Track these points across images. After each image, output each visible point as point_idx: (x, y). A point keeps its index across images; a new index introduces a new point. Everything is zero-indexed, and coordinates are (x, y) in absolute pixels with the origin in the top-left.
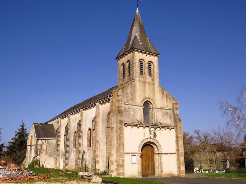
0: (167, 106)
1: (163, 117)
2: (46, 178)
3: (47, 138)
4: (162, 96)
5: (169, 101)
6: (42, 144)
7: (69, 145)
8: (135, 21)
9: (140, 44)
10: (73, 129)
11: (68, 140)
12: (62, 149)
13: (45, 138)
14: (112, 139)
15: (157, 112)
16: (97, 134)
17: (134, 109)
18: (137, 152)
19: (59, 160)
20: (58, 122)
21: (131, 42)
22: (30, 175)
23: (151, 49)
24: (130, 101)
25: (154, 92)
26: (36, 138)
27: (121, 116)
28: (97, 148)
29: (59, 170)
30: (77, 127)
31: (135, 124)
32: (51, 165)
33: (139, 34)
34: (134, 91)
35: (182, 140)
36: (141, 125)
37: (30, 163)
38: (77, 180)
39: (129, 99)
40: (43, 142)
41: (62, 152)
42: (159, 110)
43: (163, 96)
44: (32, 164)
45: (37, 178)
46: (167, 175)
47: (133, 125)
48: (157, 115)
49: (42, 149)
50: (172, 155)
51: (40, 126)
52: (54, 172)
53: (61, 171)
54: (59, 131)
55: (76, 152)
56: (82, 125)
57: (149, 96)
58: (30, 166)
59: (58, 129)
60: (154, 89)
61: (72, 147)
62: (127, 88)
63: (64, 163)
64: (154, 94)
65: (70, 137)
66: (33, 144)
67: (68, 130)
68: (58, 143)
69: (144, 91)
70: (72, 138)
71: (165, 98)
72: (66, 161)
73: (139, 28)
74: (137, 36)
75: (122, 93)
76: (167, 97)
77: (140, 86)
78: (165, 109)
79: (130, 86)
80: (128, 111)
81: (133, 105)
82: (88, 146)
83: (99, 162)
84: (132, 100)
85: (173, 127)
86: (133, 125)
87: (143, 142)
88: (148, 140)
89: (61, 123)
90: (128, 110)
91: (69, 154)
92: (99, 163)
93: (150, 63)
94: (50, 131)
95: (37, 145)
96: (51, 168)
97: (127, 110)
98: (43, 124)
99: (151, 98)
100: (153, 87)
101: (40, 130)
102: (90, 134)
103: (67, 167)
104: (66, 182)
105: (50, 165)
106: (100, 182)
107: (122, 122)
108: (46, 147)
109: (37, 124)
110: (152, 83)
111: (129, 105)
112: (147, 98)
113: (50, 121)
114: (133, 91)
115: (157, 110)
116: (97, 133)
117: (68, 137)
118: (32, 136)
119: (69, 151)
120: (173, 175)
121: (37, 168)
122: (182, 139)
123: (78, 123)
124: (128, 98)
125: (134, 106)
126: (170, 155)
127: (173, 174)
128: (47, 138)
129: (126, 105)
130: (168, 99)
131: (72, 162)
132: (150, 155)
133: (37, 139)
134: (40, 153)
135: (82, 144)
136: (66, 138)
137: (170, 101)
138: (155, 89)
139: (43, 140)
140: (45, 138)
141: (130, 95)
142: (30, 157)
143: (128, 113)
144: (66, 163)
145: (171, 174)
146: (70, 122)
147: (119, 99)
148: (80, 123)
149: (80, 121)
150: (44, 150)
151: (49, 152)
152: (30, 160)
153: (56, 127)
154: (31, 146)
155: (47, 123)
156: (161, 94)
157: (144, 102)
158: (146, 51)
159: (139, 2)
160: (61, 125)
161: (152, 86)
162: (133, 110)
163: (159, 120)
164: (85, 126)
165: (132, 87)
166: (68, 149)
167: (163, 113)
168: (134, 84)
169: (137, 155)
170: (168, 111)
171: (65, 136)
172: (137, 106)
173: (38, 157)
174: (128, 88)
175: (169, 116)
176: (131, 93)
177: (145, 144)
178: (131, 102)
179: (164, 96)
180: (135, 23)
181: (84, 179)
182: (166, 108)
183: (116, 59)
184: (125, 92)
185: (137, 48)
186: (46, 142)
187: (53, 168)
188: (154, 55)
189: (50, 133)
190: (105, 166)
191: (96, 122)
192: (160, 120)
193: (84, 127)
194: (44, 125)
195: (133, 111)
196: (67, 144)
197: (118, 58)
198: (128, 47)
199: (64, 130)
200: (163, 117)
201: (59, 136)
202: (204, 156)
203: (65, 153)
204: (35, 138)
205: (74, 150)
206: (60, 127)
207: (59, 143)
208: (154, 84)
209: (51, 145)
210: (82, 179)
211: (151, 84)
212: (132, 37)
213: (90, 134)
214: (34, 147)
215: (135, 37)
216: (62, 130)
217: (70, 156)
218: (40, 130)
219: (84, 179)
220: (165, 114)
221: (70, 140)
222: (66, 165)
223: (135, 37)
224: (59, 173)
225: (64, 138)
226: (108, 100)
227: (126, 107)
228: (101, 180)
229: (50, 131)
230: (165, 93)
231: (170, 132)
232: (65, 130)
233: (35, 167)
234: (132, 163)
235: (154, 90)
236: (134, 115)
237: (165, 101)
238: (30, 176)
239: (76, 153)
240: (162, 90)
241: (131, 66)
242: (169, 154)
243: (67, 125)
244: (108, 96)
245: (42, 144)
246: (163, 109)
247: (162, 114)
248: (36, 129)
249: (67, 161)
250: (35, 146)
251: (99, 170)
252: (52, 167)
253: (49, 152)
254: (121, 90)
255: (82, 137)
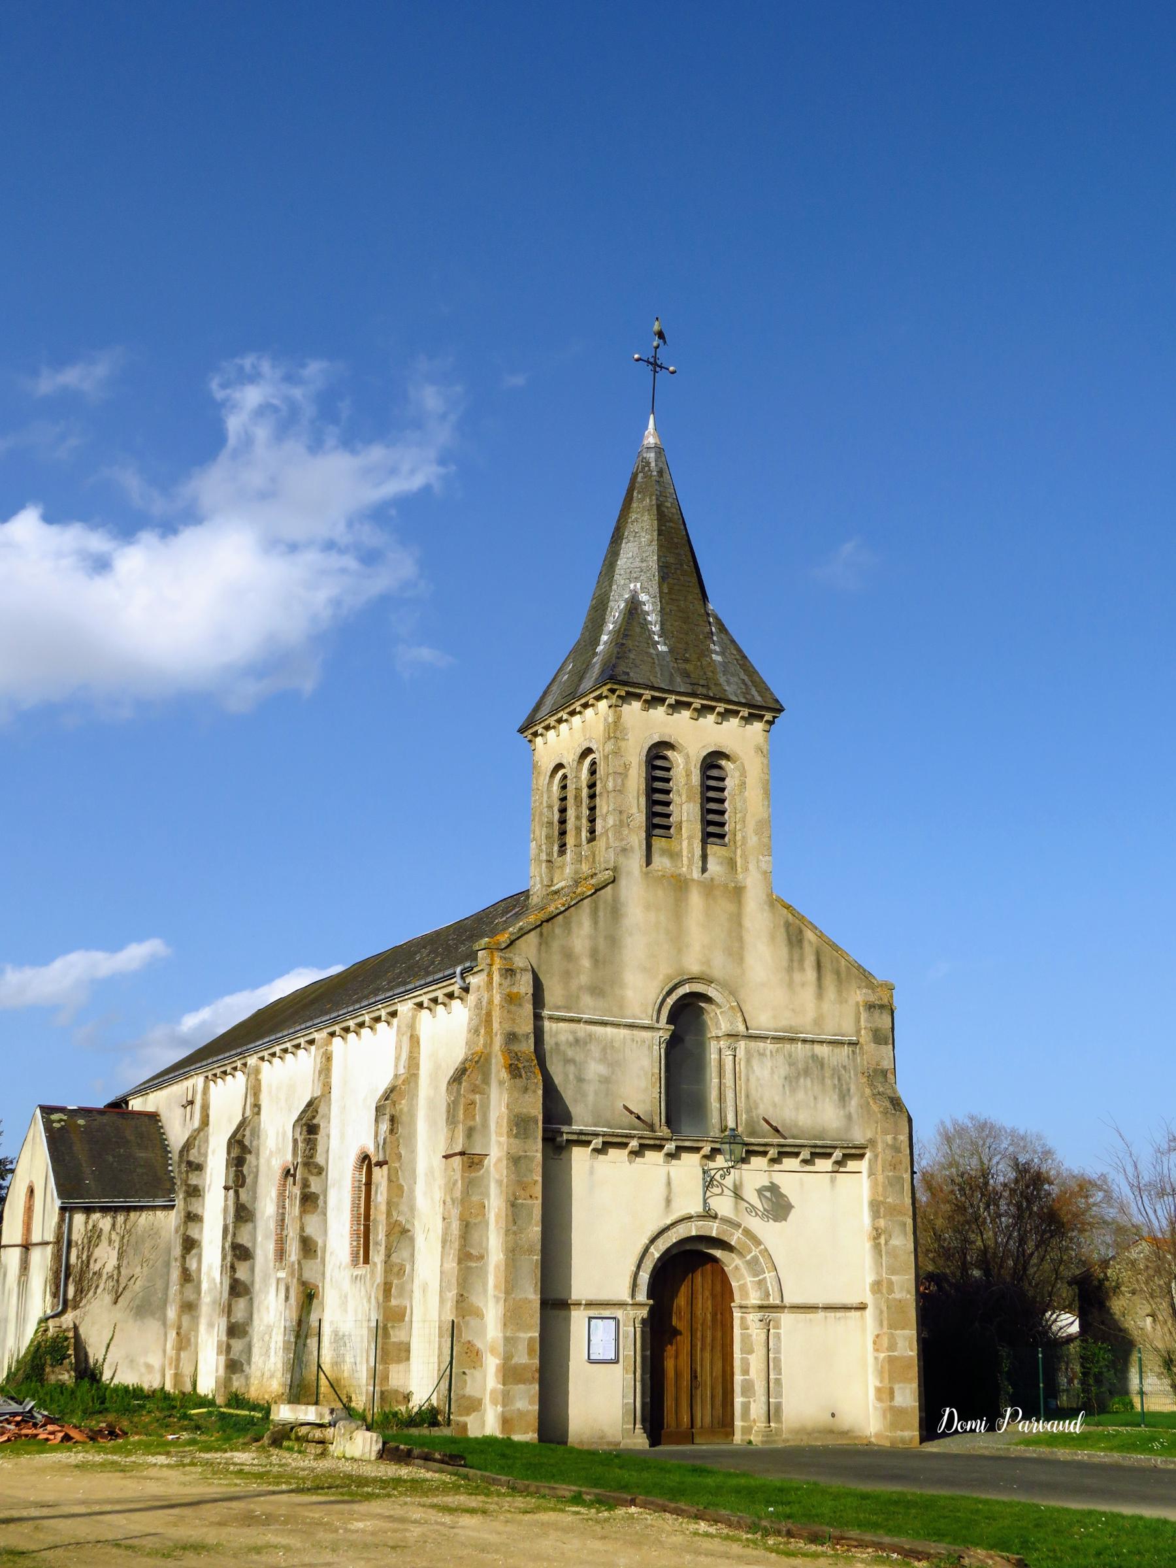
0: (818, 1021)
1: (793, 1090)
2: (104, 1437)
3: (119, 1202)
4: (791, 960)
5: (831, 992)
6: (94, 1237)
7: (249, 1245)
8: (634, 505)
9: (659, 654)
10: (274, 1149)
11: (242, 1214)
12: (210, 1267)
13: (106, 1202)
14: (473, 1220)
15: (755, 1063)
16: (401, 1187)
17: (607, 1047)
18: (625, 1296)
19: (197, 1337)
20: (191, 1103)
21: (604, 638)
22: (19, 1418)
23: (722, 679)
24: (587, 1000)
25: (740, 939)
26: (58, 1203)
27: (526, 1090)
28: (401, 1271)
29: (194, 1399)
30: (295, 1141)
31: (613, 1135)
32: (149, 1367)
33: (655, 589)
34: (614, 942)
35: (905, 1224)
36: (651, 1142)
37: (22, 1354)
38: (263, 1447)
39: (580, 988)
40: (101, 1225)
41: (210, 1290)
42: (769, 1046)
43: (794, 964)
44: (34, 1358)
45: (53, 1433)
46: (809, 1434)
47: (600, 1140)
48: (753, 1079)
49: (94, 1267)
50: (839, 1314)
51: (81, 1122)
52: (162, 1410)
53: (203, 1402)
54: (193, 1156)
55: (287, 1289)
56: (322, 1132)
57: (707, 963)
58: (18, 1370)
59: (187, 1146)
60: (737, 920)
61: (266, 1257)
62: (567, 925)
63: (222, 1358)
64: (736, 948)
65: (254, 1198)
66: (36, 1238)
67: (248, 1157)
68: (190, 1233)
69: (677, 938)
70: (267, 1207)
71: (810, 974)
72: (233, 1342)
73: (655, 547)
74: (643, 597)
75: (539, 950)
76: (819, 966)
77: (648, 907)
78: (804, 1041)
79: (588, 910)
80: (572, 1061)
81: (604, 1024)
82: (355, 1256)
83: (408, 1351)
84: (597, 991)
85: (853, 1151)
86: (600, 1140)
87: (660, 1241)
88: (693, 1229)
89: (205, 1108)
90: (570, 1053)
91: (251, 1299)
92: (408, 1359)
93: (713, 763)
94: (142, 1155)
95: (62, 1243)
96: (146, 1387)
97: (564, 1053)
98: (100, 1112)
99: (717, 972)
100: (731, 907)
101: (80, 1150)
102: (368, 1184)
103: (237, 1383)
104: (202, 1455)
105: (143, 1370)
106: (373, 1458)
107: (532, 1126)
108: (115, 1254)
109: (62, 1110)
110: (726, 886)
111: (579, 1021)
112: (691, 980)
113: (143, 1089)
114: (606, 938)
115: (753, 1044)
116: (402, 1181)
117: (244, 1196)
118: (31, 1191)
119: (253, 1282)
120: (844, 1433)
121: (62, 1386)
122: (910, 1221)
123: (299, 1119)
124: (574, 985)
125: (609, 1030)
126: (831, 1315)
127: (846, 1427)
128: (119, 1202)
129: (562, 1025)
130: (829, 981)
131: (267, 1354)
132: (709, 1317)
133: (63, 1209)
134: (80, 1291)
135: (320, 1243)
136: (231, 1203)
137: (839, 992)
138: (747, 923)
139: (96, 1216)
140: (106, 1202)
141: (586, 963)
142: (21, 1319)
143: (571, 1069)
144: (234, 1355)
145: (831, 1432)
146: (257, 1106)
147: (515, 990)
148: (309, 1114)
149: (310, 1104)
150: (104, 1277)
151: (138, 1286)
152: (19, 1338)
153: (176, 1132)
154: (26, 1247)
155: (119, 1106)
156: (784, 951)
157: (670, 1001)
158: (694, 695)
159: (662, 374)
160: (205, 1121)
161: (724, 906)
162: (604, 1050)
163: (764, 1109)
164: (342, 1135)
165: (601, 914)
166: (242, 1274)
167: (790, 1065)
168: (609, 897)
169: (619, 1313)
170: (822, 1051)
171: (227, 1188)
172: (632, 1026)
173: (68, 1319)
174: (574, 926)
175: (828, 1082)
176: (594, 954)
177: (674, 1252)
178: (589, 1007)
179: (801, 961)
180: (634, 516)
181: (298, 1439)
182: (810, 1036)
183: (522, 730)
184: (556, 945)
185: (634, 677)
186: (118, 1226)
187: (156, 1385)
188: (745, 712)
189: (139, 1170)
190: (436, 1375)
191: (393, 1119)
192: (775, 1105)
193: (334, 1143)
194: (104, 1119)
195: (603, 1059)
196: (240, 1240)
197: (530, 727)
198: (588, 666)
199: (225, 1155)
200: (793, 1090)
201: (194, 1192)
202: (1154, 1321)
203: (226, 1295)
204: (49, 1203)
205: (278, 1280)
206: (199, 1130)
207: (193, 1233)
208: (737, 892)
209: (148, 1244)
210: (290, 1443)
211: (717, 893)
212: (611, 604)
213: (368, 1184)
214: (44, 1257)
215: (634, 608)
216: (213, 1152)
217: (255, 1316)
218: (80, 1150)
219: (298, 1439)
220: (807, 1072)
221: (258, 1215)
222: (234, 1366)
223: (634, 608)
224: (189, 1418)
225: (222, 1204)
226: (456, 989)
227: (562, 1038)
228: (380, 1445)
229: (142, 1155)
230: (806, 945)
231: (833, 1181)
232: (229, 1153)
233: (52, 1379)
234: (591, 1361)
235: (740, 925)
236: (605, 1080)
237: (808, 995)
238: (18, 1424)
239: (287, 1298)
240: (788, 925)
241: (598, 783)
242: (828, 1308)
243: (242, 1125)
244: (458, 970)
245: (94, 1237)
246: (792, 1040)
247: (783, 1070)
248: (58, 1142)
249: (238, 1345)
250: (49, 1248)
251: (407, 1398)
252: (150, 1382)
253: (138, 1286)
254: (533, 937)
255: (320, 1202)
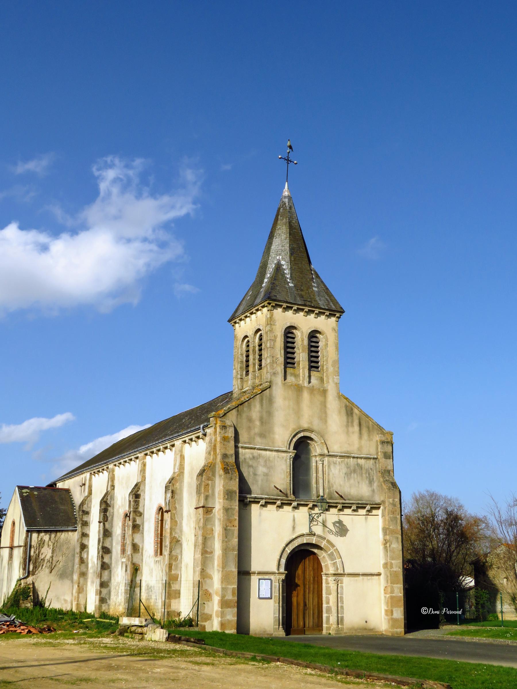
0: (360, 449)
1: (349, 479)
2: (46, 631)
3: (52, 528)
4: (348, 422)
5: (365, 436)
6: (41, 543)
7: (109, 547)
8: (279, 222)
9: (290, 287)
10: (120, 505)
11: (107, 533)
12: (92, 557)
13: (47, 528)
14: (208, 536)
15: (332, 467)
16: (176, 522)
17: (267, 460)
18: (275, 570)
19: (86, 587)
20: (84, 485)
21: (266, 280)
22: (8, 623)
23: (317, 299)
24: (258, 439)
25: (325, 413)
26: (25, 529)
27: (231, 479)
28: (176, 559)
29: (85, 615)
30: (130, 501)
31: (269, 499)
32: (66, 601)
33: (288, 259)
34: (270, 414)
35: (398, 538)
36: (286, 502)
37: (10, 595)
38: (116, 636)
39: (255, 434)
40: (44, 538)
41: (92, 567)
42: (338, 460)
43: (349, 423)
44: (15, 597)
45: (23, 630)
46: (356, 630)
47: (264, 501)
48: (331, 474)
49: (42, 557)
50: (369, 578)
51: (36, 493)
52: (71, 619)
53: (89, 616)
54: (85, 508)
55: (126, 567)
56: (142, 497)
57: (311, 423)
58: (8, 602)
59: (82, 504)
60: (324, 404)
61: (117, 552)
62: (249, 407)
63: (98, 597)
64: (324, 417)
65: (112, 526)
66: (16, 544)
67: (109, 508)
68: (84, 542)
69: (298, 412)
70: (117, 530)
71: (356, 428)
72: (102, 590)
73: (288, 240)
74: (283, 262)
75: (237, 417)
76: (360, 425)
77: (285, 399)
78: (354, 457)
79: (258, 400)
80: (251, 466)
81: (266, 450)
82: (156, 552)
83: (179, 594)
84: (262, 435)
85: (375, 506)
86: (264, 501)
87: (290, 545)
88: (304, 540)
89: (90, 487)
90: (251, 463)
91: (110, 571)
92: (179, 597)
93: (313, 335)
94: (62, 507)
95: (27, 546)
96: (64, 609)
97: (248, 463)
98: (44, 489)
99: (315, 427)
100: (321, 399)
101: (35, 506)
102: (162, 520)
103: (104, 608)
104: (89, 639)
105: (63, 602)
106: (164, 641)
107: (234, 495)
108: (50, 551)
109: (27, 488)
110: (319, 389)
111: (254, 449)
112: (304, 431)
113: (63, 479)
114: (266, 412)
115: (331, 459)
116: (177, 519)
117: (107, 526)
118: (14, 523)
119: (111, 563)
120: (371, 630)
121: (27, 609)
122: (400, 537)
123: (132, 492)
124: (252, 433)
125: (268, 453)
126: (365, 578)
127: (372, 627)
128: (52, 528)
129: (247, 450)
130: (365, 431)
131: (117, 595)
132: (312, 579)
133: (28, 531)
134: (35, 567)
135: (141, 546)
136: (101, 528)
137: (369, 436)
138: (329, 405)
139: (42, 534)
140: (47, 528)
141: (258, 423)
142: (9, 580)
143: (251, 470)
144: (103, 595)
145: (365, 629)
146: (113, 486)
147: (226, 435)
148: (136, 489)
149: (136, 485)
150: (46, 561)
151: (60, 565)
152: (8, 588)
153: (78, 498)
154: (12, 548)
155: (52, 486)
156: (345, 418)
157: (295, 440)
158: (305, 305)
159: (291, 164)
160: (90, 493)
161: (318, 398)
162: (266, 461)
163: (336, 487)
164: (151, 499)
165: (264, 401)
166: (106, 560)
167: (347, 468)
168: (268, 394)
169: (272, 577)
170: (361, 462)
171: (100, 522)
172: (278, 451)
173: (30, 580)
174: (252, 407)
175: (364, 475)
176: (261, 419)
177: (296, 550)
178: (259, 442)
179: (352, 422)
180: (279, 227)
181: (131, 632)
182: (356, 455)
183: (229, 321)
184: (244, 415)
185: (279, 297)
186: (52, 539)
187: (69, 609)
188: (327, 313)
189: (61, 514)
190: (192, 604)
191: (173, 492)
192: (341, 486)
193: (147, 502)
194: (46, 492)
195: (265, 465)
196: (105, 545)
197: (233, 319)
198: (259, 293)
199: (99, 508)
200: (349, 479)
201: (85, 524)
202: (507, 580)
203: (99, 569)
204: (21, 529)
205: (122, 562)
206: (87, 497)
207: (85, 542)
208: (324, 392)
209: (65, 547)
210: (128, 634)
211: (315, 392)
212: (269, 265)
213: (162, 520)
214: (19, 552)
215: (279, 267)
216: (94, 506)
217: (112, 578)
218: (35, 506)
219: (131, 632)
220: (355, 471)
221: (114, 534)
222: (103, 600)
223: (279, 267)
224: (83, 623)
225: (98, 529)
226: (200, 434)
227: (247, 456)
228: (167, 635)
229: (62, 507)
230: (354, 415)
231: (366, 519)
232: (100, 507)
233: (23, 606)
234: (260, 598)
235: (325, 406)
236: (266, 475)
237: (355, 437)
238: (8, 626)
239: (126, 570)
240: (346, 407)
241: (263, 344)
242: (364, 575)
243: (106, 494)
244: (202, 426)
245: (41, 543)
246: (348, 457)
247: (344, 470)
248: (25, 502)
249: (104, 591)
250: (22, 549)
251: (179, 614)
252: (66, 607)
253: (60, 565)
254: (234, 412)
255: (141, 528)
